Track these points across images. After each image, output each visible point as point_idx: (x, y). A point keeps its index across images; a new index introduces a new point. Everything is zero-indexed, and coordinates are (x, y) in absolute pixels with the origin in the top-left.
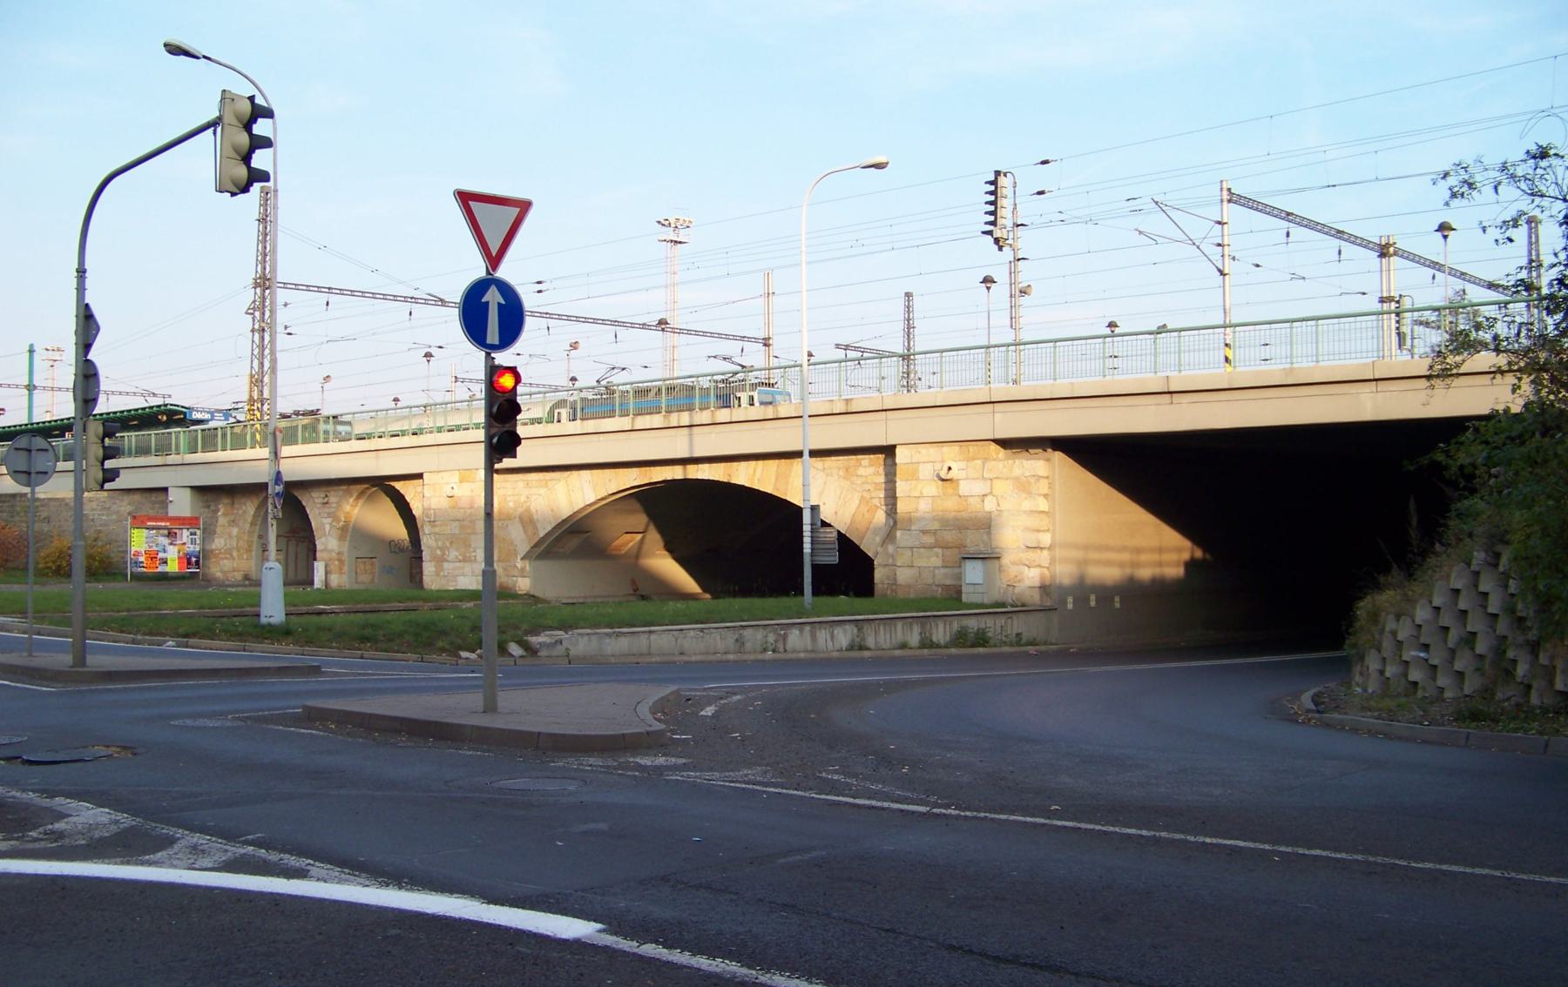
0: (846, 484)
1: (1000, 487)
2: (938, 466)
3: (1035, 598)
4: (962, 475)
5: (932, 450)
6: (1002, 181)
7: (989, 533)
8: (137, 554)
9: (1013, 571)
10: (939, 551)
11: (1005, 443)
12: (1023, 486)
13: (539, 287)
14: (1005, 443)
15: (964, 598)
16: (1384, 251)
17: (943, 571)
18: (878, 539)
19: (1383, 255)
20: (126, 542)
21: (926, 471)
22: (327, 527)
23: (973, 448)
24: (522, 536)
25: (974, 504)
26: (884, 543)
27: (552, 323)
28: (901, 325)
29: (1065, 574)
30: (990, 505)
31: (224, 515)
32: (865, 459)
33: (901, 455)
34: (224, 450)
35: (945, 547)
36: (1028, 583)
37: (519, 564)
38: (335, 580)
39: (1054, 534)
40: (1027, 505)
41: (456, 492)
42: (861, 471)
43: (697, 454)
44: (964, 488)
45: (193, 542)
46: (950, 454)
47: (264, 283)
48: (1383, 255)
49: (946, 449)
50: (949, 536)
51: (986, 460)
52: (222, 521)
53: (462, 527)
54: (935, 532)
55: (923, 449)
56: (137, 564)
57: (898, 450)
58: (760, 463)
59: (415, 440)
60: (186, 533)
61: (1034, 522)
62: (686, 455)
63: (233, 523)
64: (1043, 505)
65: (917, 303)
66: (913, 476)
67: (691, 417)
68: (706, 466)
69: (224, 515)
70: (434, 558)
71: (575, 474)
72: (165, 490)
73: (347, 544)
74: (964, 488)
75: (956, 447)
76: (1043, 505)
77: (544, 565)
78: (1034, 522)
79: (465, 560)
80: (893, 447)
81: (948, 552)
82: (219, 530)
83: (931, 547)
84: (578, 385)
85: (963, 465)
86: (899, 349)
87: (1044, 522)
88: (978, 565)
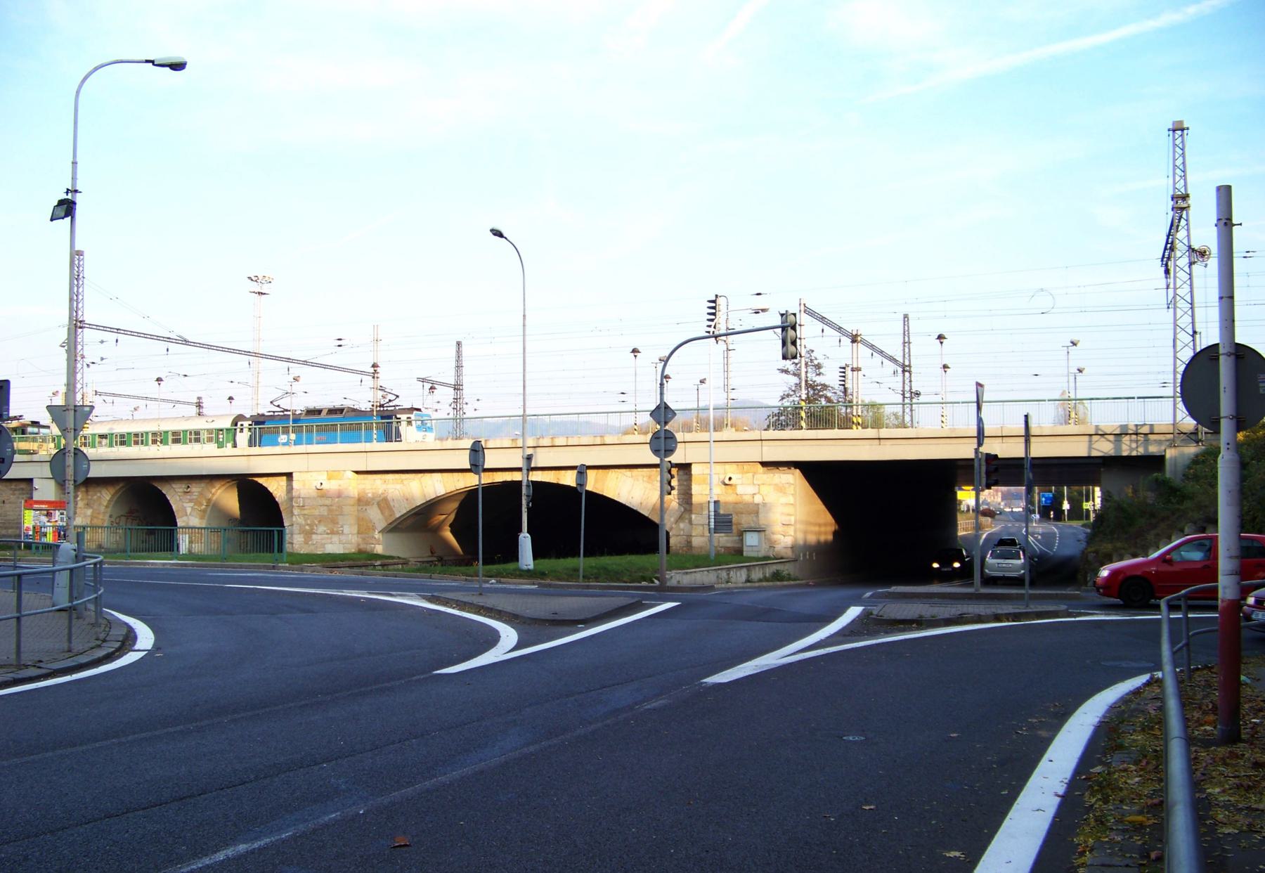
0: (649, 486)
1: (764, 489)
2: (722, 477)
3: (789, 553)
4: (739, 482)
6: (720, 301)
7: (757, 516)
8: (28, 529)
9: (777, 537)
11: (764, 464)
12: (781, 489)
14: (764, 464)
16: (854, 339)
19: (854, 341)
20: (18, 523)
22: (189, 510)
23: (746, 467)
24: (380, 516)
25: (747, 499)
28: (454, 364)
29: (800, 538)
30: (758, 499)
33: (695, 470)
36: (783, 545)
37: (377, 535)
38: (197, 548)
39: (792, 517)
40: (783, 500)
41: (325, 486)
44: (740, 490)
45: (62, 520)
46: (730, 470)
47: (76, 325)
48: (854, 341)
49: (727, 466)
51: (755, 473)
52: (80, 504)
53: (330, 511)
56: (27, 536)
57: (693, 467)
60: (57, 513)
61: (786, 510)
63: (88, 505)
64: (791, 500)
65: (464, 349)
68: (540, 473)
70: (303, 532)
71: (428, 475)
72: (31, 480)
74: (740, 490)
75: (734, 466)
76: (791, 500)
77: (391, 535)
78: (786, 510)
79: (333, 533)
87: (791, 510)
88: (755, 535)
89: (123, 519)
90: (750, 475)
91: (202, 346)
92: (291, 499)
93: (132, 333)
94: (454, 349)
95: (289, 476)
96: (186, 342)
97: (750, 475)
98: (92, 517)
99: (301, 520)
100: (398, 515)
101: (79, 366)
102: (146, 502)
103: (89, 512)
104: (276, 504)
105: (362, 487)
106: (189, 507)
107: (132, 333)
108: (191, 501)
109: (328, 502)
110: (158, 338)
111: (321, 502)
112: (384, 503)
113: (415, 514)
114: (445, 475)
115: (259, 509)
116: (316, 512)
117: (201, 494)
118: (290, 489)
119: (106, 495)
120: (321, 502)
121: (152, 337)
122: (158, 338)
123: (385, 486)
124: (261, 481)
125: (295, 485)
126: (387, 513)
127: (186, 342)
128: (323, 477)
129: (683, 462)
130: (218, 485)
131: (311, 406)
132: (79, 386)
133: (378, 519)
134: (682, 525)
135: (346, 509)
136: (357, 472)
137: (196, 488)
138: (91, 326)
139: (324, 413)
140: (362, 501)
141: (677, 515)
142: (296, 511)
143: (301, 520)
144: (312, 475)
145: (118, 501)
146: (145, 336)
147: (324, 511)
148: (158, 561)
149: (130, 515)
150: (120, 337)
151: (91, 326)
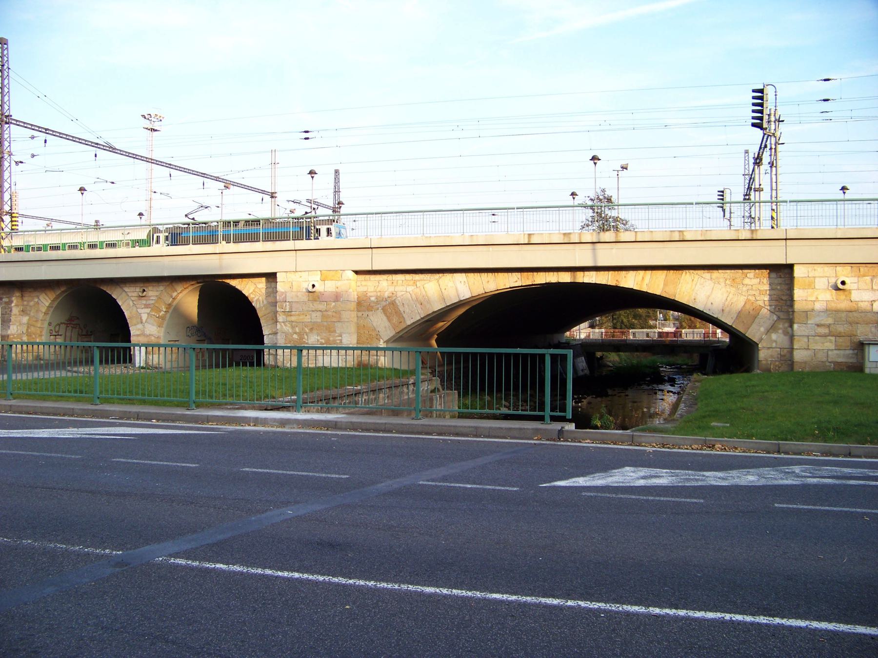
2: (832, 281)
4: (855, 286)
5: (827, 268)
10: (833, 338)
13: (307, 135)
15: (867, 371)
17: (835, 352)
18: (762, 329)
21: (822, 284)
22: (144, 317)
23: (863, 269)
24: (387, 323)
25: (864, 306)
26: (768, 332)
27: (173, 172)
31: (17, 305)
32: (751, 273)
33: (798, 272)
34: (308, 238)
35: (838, 335)
42: (746, 281)
43: (601, 263)
44: (855, 296)
46: (844, 274)
48: (272, 197)
49: (839, 268)
50: (841, 329)
52: (15, 311)
53: (323, 316)
54: (829, 326)
55: (819, 268)
57: (796, 268)
58: (649, 273)
59: (54, 254)
62: (590, 263)
63: (24, 312)
65: (342, 177)
66: (810, 285)
67: (617, 236)
68: (593, 273)
69: (17, 305)
71: (501, 275)
73: (163, 329)
74: (855, 296)
75: (848, 268)
80: (790, 267)
81: (840, 340)
82: (13, 318)
83: (825, 336)
84: (848, 196)
85: (855, 279)
86: (782, 207)
89: (63, 326)
90: (868, 279)
91: (128, 155)
92: (274, 304)
93: (60, 135)
94: (333, 176)
95: (271, 277)
96: (112, 149)
97: (868, 279)
98: (29, 325)
99: (287, 328)
100: (409, 322)
101: (6, 164)
102: (93, 309)
103: (25, 319)
104: (254, 310)
105: (362, 289)
106: (144, 313)
107: (60, 135)
108: (147, 306)
109: (322, 307)
110: (86, 143)
111: (312, 306)
112: (390, 307)
113: (427, 321)
114: (471, 275)
115: (228, 319)
116: (307, 319)
117: (159, 298)
118: (272, 290)
119: (45, 301)
120: (312, 306)
121: (79, 141)
122: (86, 143)
123: (391, 289)
124: (233, 283)
125: (280, 287)
126: (395, 320)
127: (112, 149)
128: (315, 279)
129: (782, 261)
130: (179, 287)
131: (227, 218)
132: (6, 185)
133: (384, 329)
134: (774, 336)
135: (345, 315)
136: (357, 272)
137: (153, 292)
138: (18, 123)
139: (241, 224)
140: (363, 305)
141: (768, 324)
142: (280, 318)
143: (287, 328)
144: (294, 281)
145: (58, 308)
146: (74, 139)
147: (317, 317)
148: (117, 370)
149: (70, 322)
150: (49, 138)
151: (18, 123)
